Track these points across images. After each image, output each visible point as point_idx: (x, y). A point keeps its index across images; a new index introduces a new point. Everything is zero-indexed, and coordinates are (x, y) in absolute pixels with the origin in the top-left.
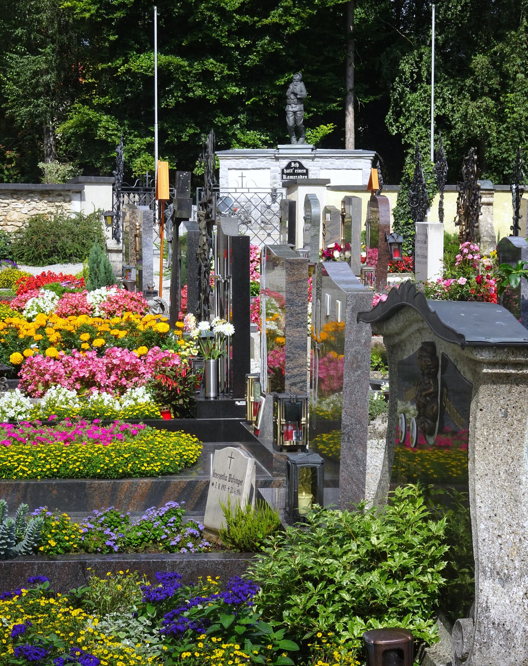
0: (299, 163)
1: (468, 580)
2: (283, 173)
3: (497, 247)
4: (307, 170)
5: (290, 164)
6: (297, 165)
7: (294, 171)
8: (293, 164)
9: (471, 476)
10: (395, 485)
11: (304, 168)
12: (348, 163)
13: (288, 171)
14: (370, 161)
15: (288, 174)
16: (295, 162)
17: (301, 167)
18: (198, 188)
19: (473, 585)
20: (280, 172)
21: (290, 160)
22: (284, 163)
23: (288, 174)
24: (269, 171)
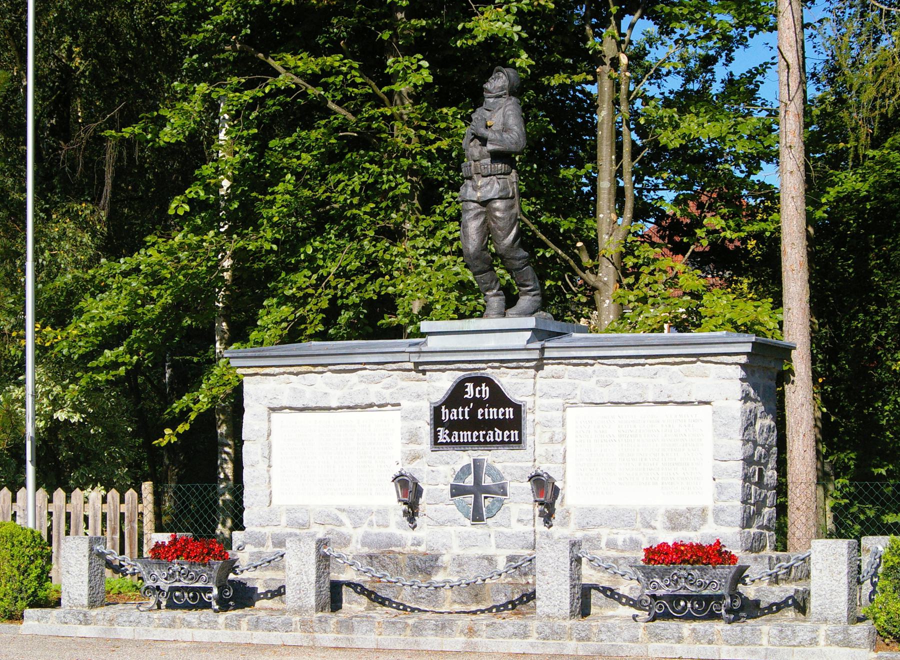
0: (489, 382)
2: (437, 421)
4: (518, 409)
5: (459, 387)
8: (470, 386)
9: (806, 265)
10: (761, 389)
12: (659, 380)
13: (457, 414)
14: (739, 373)
17: (498, 398)
20: (428, 416)
21: (461, 374)
22: (442, 384)
23: (453, 426)
24: (391, 416)
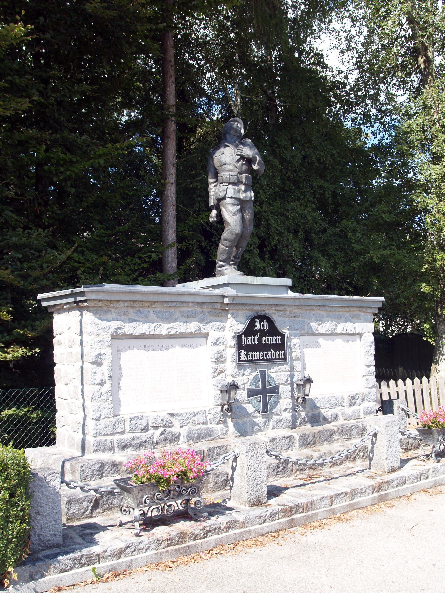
2: (240, 346)
7: (260, 340)
8: (257, 324)
15: (250, 348)
17: (273, 330)
18: (261, 396)
20: (233, 342)
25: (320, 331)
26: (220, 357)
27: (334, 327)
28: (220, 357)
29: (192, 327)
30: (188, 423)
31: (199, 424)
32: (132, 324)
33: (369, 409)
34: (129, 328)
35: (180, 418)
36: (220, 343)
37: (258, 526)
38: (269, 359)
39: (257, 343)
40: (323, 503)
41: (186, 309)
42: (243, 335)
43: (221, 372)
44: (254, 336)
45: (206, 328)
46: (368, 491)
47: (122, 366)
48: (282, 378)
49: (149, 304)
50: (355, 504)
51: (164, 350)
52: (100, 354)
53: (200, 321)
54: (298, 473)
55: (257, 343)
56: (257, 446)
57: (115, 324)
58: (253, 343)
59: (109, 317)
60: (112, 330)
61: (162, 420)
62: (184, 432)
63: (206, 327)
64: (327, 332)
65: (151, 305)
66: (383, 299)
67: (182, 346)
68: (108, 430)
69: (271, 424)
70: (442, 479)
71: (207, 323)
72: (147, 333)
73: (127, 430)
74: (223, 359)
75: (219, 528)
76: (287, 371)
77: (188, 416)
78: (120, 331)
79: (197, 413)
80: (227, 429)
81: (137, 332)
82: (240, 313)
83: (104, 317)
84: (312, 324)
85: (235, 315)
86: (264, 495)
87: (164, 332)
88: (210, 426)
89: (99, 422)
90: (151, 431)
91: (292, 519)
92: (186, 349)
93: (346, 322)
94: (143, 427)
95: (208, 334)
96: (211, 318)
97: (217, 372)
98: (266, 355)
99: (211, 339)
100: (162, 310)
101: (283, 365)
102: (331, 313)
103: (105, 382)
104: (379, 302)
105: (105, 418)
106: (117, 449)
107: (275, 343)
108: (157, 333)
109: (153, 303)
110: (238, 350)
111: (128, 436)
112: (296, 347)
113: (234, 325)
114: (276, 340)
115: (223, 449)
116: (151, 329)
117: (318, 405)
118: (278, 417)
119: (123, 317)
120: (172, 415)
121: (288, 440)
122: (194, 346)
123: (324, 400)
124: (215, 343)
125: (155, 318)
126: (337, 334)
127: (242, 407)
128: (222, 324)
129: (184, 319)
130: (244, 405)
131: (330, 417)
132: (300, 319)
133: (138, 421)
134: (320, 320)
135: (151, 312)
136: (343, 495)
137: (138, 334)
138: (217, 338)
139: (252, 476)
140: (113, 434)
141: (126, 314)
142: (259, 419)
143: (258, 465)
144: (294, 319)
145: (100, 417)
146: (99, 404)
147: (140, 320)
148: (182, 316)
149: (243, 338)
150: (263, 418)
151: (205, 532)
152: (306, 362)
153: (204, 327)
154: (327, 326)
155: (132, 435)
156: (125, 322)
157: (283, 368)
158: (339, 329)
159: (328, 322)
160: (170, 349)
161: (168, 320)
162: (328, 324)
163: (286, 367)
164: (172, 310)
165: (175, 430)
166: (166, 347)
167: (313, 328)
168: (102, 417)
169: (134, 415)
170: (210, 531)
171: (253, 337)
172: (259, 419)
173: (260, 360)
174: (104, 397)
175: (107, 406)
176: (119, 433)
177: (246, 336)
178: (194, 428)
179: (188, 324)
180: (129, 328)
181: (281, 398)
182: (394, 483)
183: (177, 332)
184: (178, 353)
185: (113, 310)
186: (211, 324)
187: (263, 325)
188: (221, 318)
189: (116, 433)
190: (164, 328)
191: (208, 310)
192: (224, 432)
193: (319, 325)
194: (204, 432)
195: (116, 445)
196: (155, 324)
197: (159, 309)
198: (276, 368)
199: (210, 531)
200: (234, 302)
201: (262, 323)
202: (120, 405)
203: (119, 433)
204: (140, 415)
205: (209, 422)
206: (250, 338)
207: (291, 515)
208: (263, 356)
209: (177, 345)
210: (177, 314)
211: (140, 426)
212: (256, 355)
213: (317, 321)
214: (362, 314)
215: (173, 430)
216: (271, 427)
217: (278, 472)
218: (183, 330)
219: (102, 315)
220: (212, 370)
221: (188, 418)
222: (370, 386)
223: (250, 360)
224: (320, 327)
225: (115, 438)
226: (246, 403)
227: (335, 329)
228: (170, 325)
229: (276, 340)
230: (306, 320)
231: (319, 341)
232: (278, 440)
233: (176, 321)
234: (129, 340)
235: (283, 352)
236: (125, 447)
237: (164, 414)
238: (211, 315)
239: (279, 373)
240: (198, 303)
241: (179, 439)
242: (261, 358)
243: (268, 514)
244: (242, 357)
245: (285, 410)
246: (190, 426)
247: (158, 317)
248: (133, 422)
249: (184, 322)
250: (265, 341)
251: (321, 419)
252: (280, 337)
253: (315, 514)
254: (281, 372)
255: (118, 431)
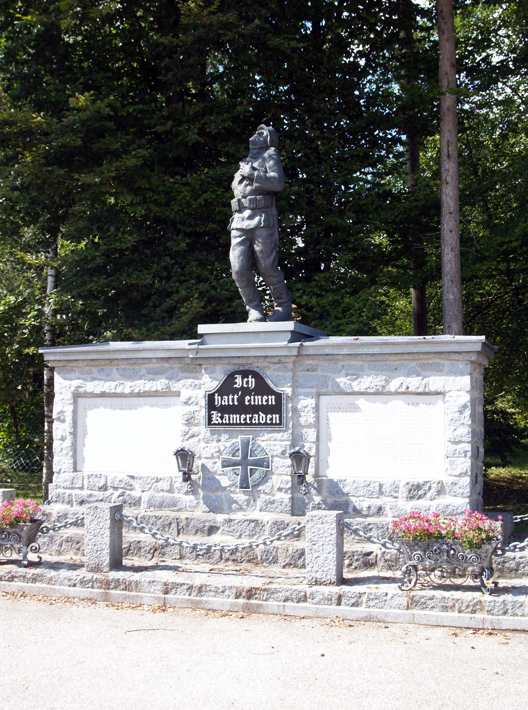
1: (447, 332)
2: (211, 405)
3: (238, 169)
5: (230, 378)
6: (252, 382)
7: (241, 400)
8: (239, 380)
11: (269, 391)
15: (224, 410)
16: (245, 374)
17: (262, 388)
18: (249, 467)
19: (461, 246)
20: (203, 402)
21: (231, 368)
23: (224, 410)
25: (356, 389)
26: (191, 418)
27: (383, 383)
28: (191, 418)
29: (159, 384)
30: (150, 488)
31: (162, 490)
32: (94, 382)
33: (451, 508)
34: (91, 387)
35: (141, 481)
36: (192, 403)
37: (67, 588)
38: (255, 424)
39: (236, 403)
40: (153, 587)
41: (151, 366)
42: (216, 395)
43: (193, 436)
44: (233, 395)
45: (176, 386)
46: (227, 593)
47: (88, 424)
48: (275, 448)
49: (107, 362)
50: (200, 602)
51: (131, 409)
52: (62, 412)
53: (169, 378)
54: (230, 563)
55: (236, 403)
56: (99, 510)
57: (76, 383)
58: (231, 403)
59: (72, 376)
60: (72, 389)
61: (120, 481)
62: (145, 497)
63: (176, 384)
64: (369, 390)
65: (111, 362)
66: (483, 338)
67: (152, 406)
68: (67, 484)
69: (259, 503)
70: (386, 615)
71: (178, 380)
72: (108, 391)
73: (86, 487)
74: (196, 421)
75: (24, 577)
76: (285, 440)
77: (149, 480)
78: (81, 390)
79: (161, 479)
80: (197, 501)
81: (98, 391)
82: (218, 368)
83: (68, 376)
84: (338, 380)
85: (209, 371)
86: (105, 564)
87: (127, 391)
88: (176, 495)
89: (60, 475)
90: (110, 491)
91: (107, 593)
92: (156, 409)
93: (408, 375)
94: (101, 485)
95: (179, 392)
96: (184, 375)
97: (188, 436)
98: (251, 419)
99: (183, 398)
100: (127, 367)
101: (279, 431)
102: (378, 363)
103: (66, 438)
104: (475, 342)
105: (65, 472)
106: (75, 503)
107: (265, 403)
108: (118, 391)
109: (111, 360)
110: (209, 412)
111: (85, 493)
112: (306, 410)
113: (210, 383)
114: (267, 401)
115: (161, 520)
116: (112, 388)
117: (345, 491)
118: (268, 497)
119: (85, 376)
120: (132, 477)
121: (253, 524)
122: (167, 406)
123: (356, 485)
124: (186, 403)
125: (118, 376)
126: (390, 393)
127: (215, 478)
128: (197, 382)
129: (150, 376)
130: (217, 477)
131: (365, 509)
132: (319, 373)
133: (96, 479)
134: (356, 375)
135: (115, 370)
136: (185, 587)
137: (98, 392)
138: (187, 397)
139: (92, 541)
140: (72, 488)
141: (90, 372)
142: (240, 496)
143: (99, 530)
144: (308, 373)
145: (60, 471)
146: (60, 458)
147: (103, 378)
148: (149, 373)
149: (216, 397)
150: (245, 495)
151: (10, 575)
152: (332, 430)
153: (174, 385)
154: (368, 382)
155: (90, 492)
156: (86, 381)
157: (278, 436)
158: (393, 386)
159: (369, 376)
160: (139, 409)
161: (132, 377)
162: (370, 379)
163: (286, 435)
164: (137, 367)
165: (136, 494)
166: (134, 407)
167: (342, 385)
168: (62, 471)
169: (91, 473)
170: (16, 577)
171: (231, 397)
172: (239, 495)
173: (241, 424)
174: (64, 452)
175: (67, 461)
176: (79, 488)
177: (221, 395)
178: (156, 494)
179: (154, 382)
180: (91, 387)
181: (273, 474)
182: (280, 595)
183: (140, 390)
184: (147, 413)
185: (76, 369)
186: (182, 382)
187: (247, 383)
188: (198, 374)
189: (75, 488)
190: (127, 387)
191: (179, 366)
192: (193, 505)
193: (354, 380)
194: (167, 501)
195: (74, 499)
196: (117, 382)
197: (122, 367)
198: (267, 436)
199: (16, 577)
200: (198, 356)
201: (246, 379)
202: (84, 462)
203: (79, 488)
204: (99, 473)
205: (176, 491)
206: (226, 397)
207: (109, 589)
208: (245, 419)
209: (146, 405)
210: (143, 371)
211: (97, 484)
212: (235, 418)
213: (347, 375)
214: (447, 363)
215: (133, 493)
216: (258, 508)
217: (199, 555)
218: (147, 389)
219: (66, 374)
220: (181, 433)
221: (149, 483)
222: (456, 474)
223: (226, 424)
224: (354, 384)
225: (74, 492)
226: (220, 475)
227: (384, 387)
228: (133, 383)
229: (267, 401)
230: (329, 374)
231: (357, 402)
232: (236, 522)
233: (140, 378)
234: (96, 398)
235: (278, 416)
236: (82, 503)
237: (123, 476)
238: (183, 371)
239: (271, 442)
240: (162, 359)
241: (140, 504)
242: (243, 422)
243: (79, 578)
244: (214, 419)
245: (280, 489)
246: (152, 492)
247: (121, 375)
248: (91, 480)
249: (150, 380)
250: (250, 401)
251: (350, 510)
252: (273, 397)
253: (138, 596)
254: (275, 440)
255: (77, 486)
